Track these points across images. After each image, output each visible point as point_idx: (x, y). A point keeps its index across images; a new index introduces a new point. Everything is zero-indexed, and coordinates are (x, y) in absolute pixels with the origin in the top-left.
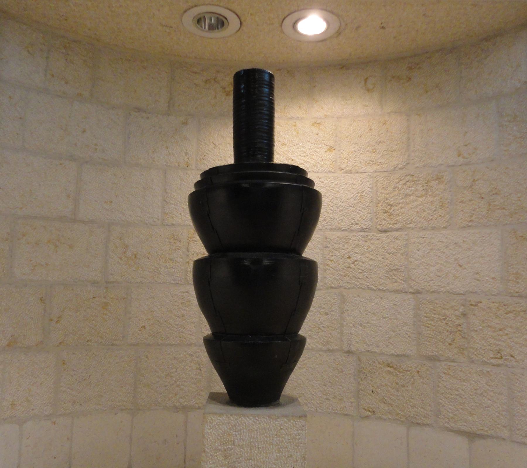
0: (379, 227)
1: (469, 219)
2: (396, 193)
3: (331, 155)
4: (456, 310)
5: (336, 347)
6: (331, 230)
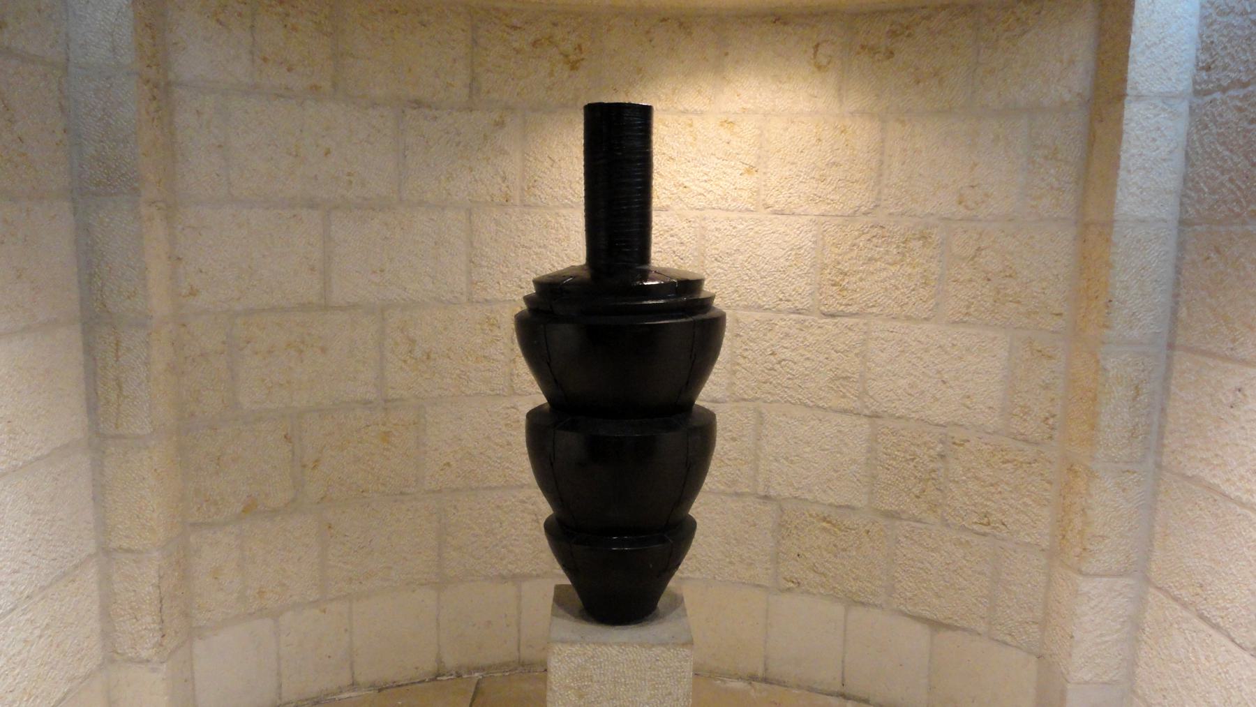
1: (964, 311)
2: (854, 254)
3: (748, 182)
4: (929, 448)
6: (746, 308)
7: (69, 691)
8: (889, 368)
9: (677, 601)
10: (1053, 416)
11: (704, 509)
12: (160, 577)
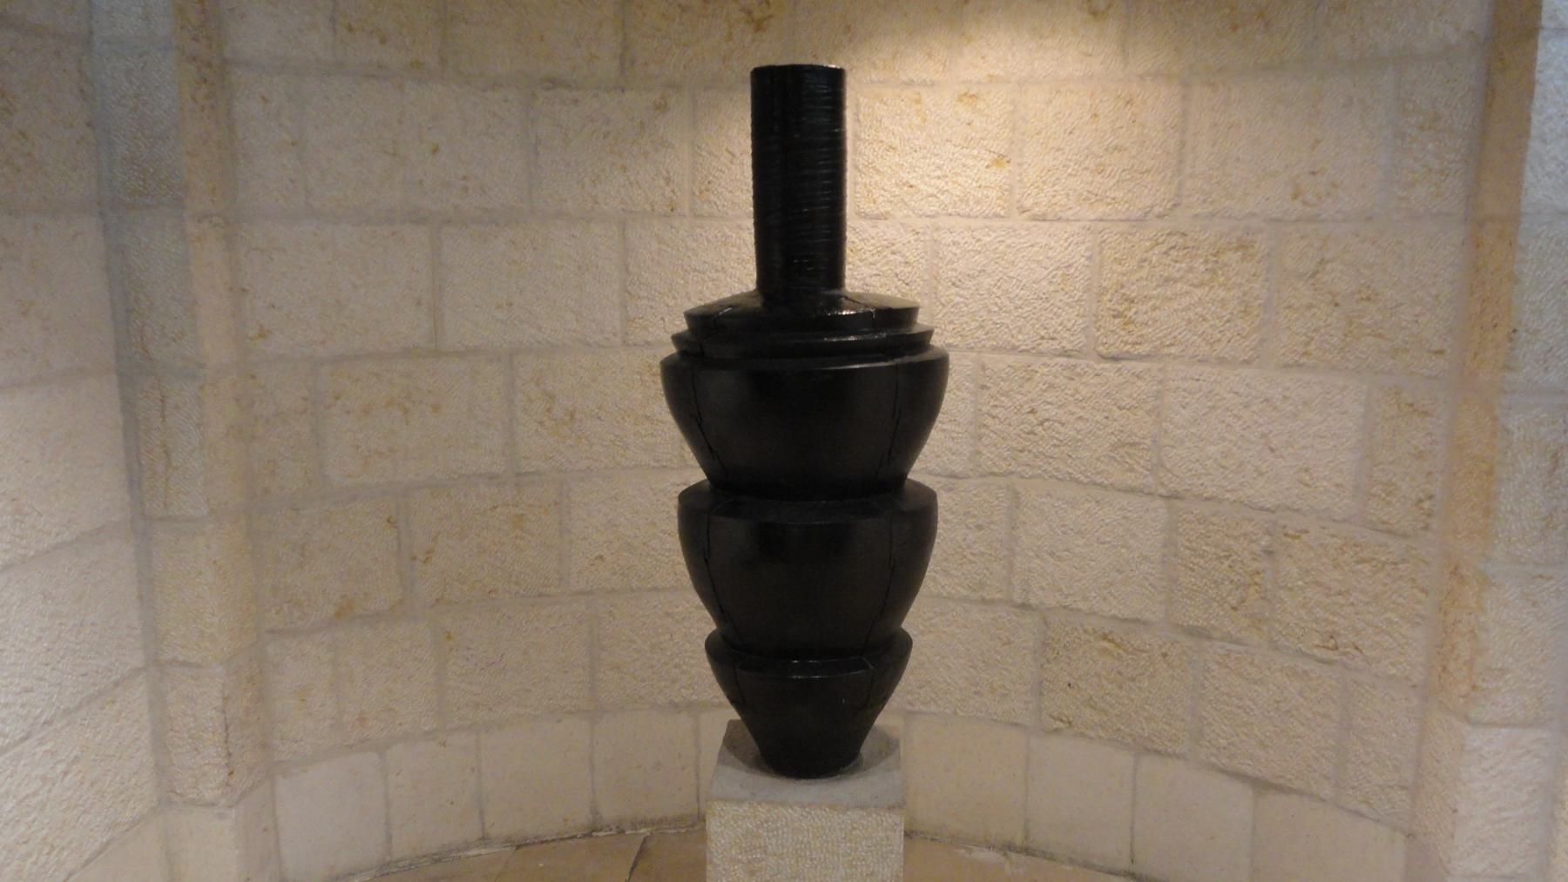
0: (1101, 348)
1: (1301, 349)
2: (1144, 273)
4: (1252, 541)
5: (998, 596)
6: (995, 349)
7: (108, 843)
8: (1193, 430)
9: (889, 746)
10: (1431, 497)
11: (920, 620)
12: (226, 699)
